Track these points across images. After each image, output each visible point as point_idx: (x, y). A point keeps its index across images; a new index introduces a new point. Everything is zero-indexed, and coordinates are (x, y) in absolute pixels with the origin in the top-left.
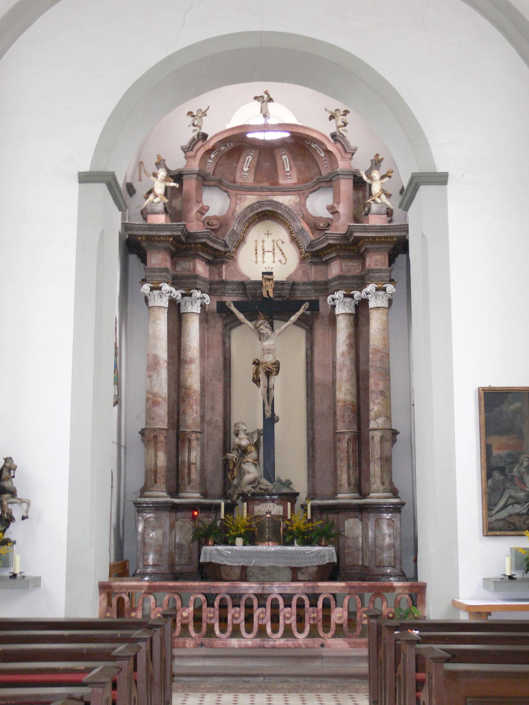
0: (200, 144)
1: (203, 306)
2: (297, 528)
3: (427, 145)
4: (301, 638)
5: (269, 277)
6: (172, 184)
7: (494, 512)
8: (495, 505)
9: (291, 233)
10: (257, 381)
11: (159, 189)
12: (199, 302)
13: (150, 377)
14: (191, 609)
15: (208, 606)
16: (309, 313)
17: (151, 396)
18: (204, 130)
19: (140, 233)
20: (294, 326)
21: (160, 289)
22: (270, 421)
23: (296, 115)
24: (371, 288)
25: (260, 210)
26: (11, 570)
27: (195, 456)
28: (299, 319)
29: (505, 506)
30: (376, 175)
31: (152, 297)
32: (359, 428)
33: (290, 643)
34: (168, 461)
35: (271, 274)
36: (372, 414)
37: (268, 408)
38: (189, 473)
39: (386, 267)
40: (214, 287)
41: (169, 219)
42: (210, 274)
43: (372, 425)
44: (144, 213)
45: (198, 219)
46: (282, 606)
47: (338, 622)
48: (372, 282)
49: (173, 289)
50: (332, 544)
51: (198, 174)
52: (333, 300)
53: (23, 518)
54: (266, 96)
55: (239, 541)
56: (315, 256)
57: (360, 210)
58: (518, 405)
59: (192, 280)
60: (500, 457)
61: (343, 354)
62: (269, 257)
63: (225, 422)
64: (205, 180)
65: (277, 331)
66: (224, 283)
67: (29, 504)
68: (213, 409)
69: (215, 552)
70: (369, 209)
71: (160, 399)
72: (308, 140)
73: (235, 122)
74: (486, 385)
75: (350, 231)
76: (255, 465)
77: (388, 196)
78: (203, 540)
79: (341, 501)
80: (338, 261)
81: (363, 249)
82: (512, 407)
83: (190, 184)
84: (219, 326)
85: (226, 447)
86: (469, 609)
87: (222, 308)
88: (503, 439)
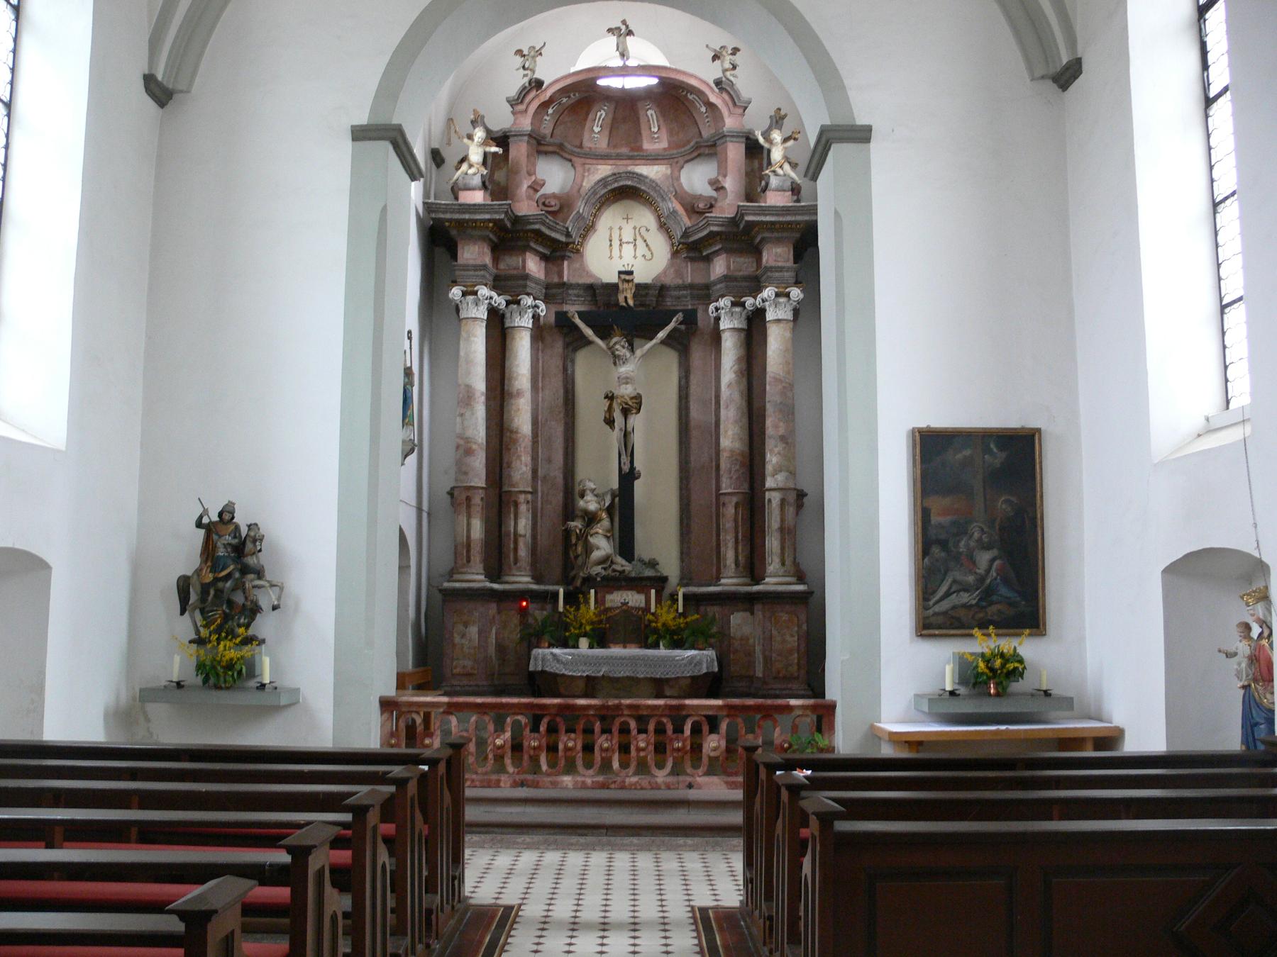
0: (533, 93)
1: (536, 317)
2: (664, 625)
3: (843, 88)
4: (661, 776)
5: (627, 277)
6: (494, 149)
7: (931, 603)
8: (934, 592)
9: (659, 217)
10: (610, 422)
11: (476, 155)
12: (530, 312)
13: (462, 415)
14: (508, 735)
15: (532, 731)
16: (683, 327)
17: (462, 442)
18: (537, 75)
19: (448, 216)
20: (664, 348)
21: (475, 293)
22: (628, 478)
23: (667, 55)
24: (768, 292)
25: (616, 185)
26: (258, 679)
27: (524, 525)
28: (669, 336)
29: (947, 595)
30: (777, 136)
31: (464, 306)
32: (752, 488)
33: (645, 780)
34: (487, 531)
35: (631, 273)
36: (769, 468)
37: (625, 459)
38: (516, 549)
39: (790, 263)
40: (552, 292)
41: (489, 197)
42: (547, 274)
43: (770, 483)
44: (455, 191)
45: (529, 198)
46: (634, 732)
47: (712, 754)
48: (770, 284)
49: (494, 294)
50: (712, 646)
51: (530, 136)
52: (717, 309)
53: (275, 608)
54: (623, 28)
55: (584, 642)
56: (691, 249)
57: (754, 185)
58: (967, 452)
59: (521, 282)
60: (941, 526)
61: (729, 385)
62: (628, 249)
63: (565, 478)
64: (540, 146)
65: (639, 352)
66: (563, 285)
67: (282, 589)
68: (549, 461)
69: (549, 657)
70: (767, 184)
71: (474, 447)
72: (683, 89)
73: (584, 62)
74: (922, 424)
75: (741, 212)
76: (608, 538)
77: (794, 166)
78: (534, 640)
79: (726, 588)
80: (724, 256)
81: (758, 240)
82: (959, 456)
83: (519, 150)
84: (559, 346)
85: (569, 511)
86: (895, 738)
87: (563, 323)
88: (946, 501)
